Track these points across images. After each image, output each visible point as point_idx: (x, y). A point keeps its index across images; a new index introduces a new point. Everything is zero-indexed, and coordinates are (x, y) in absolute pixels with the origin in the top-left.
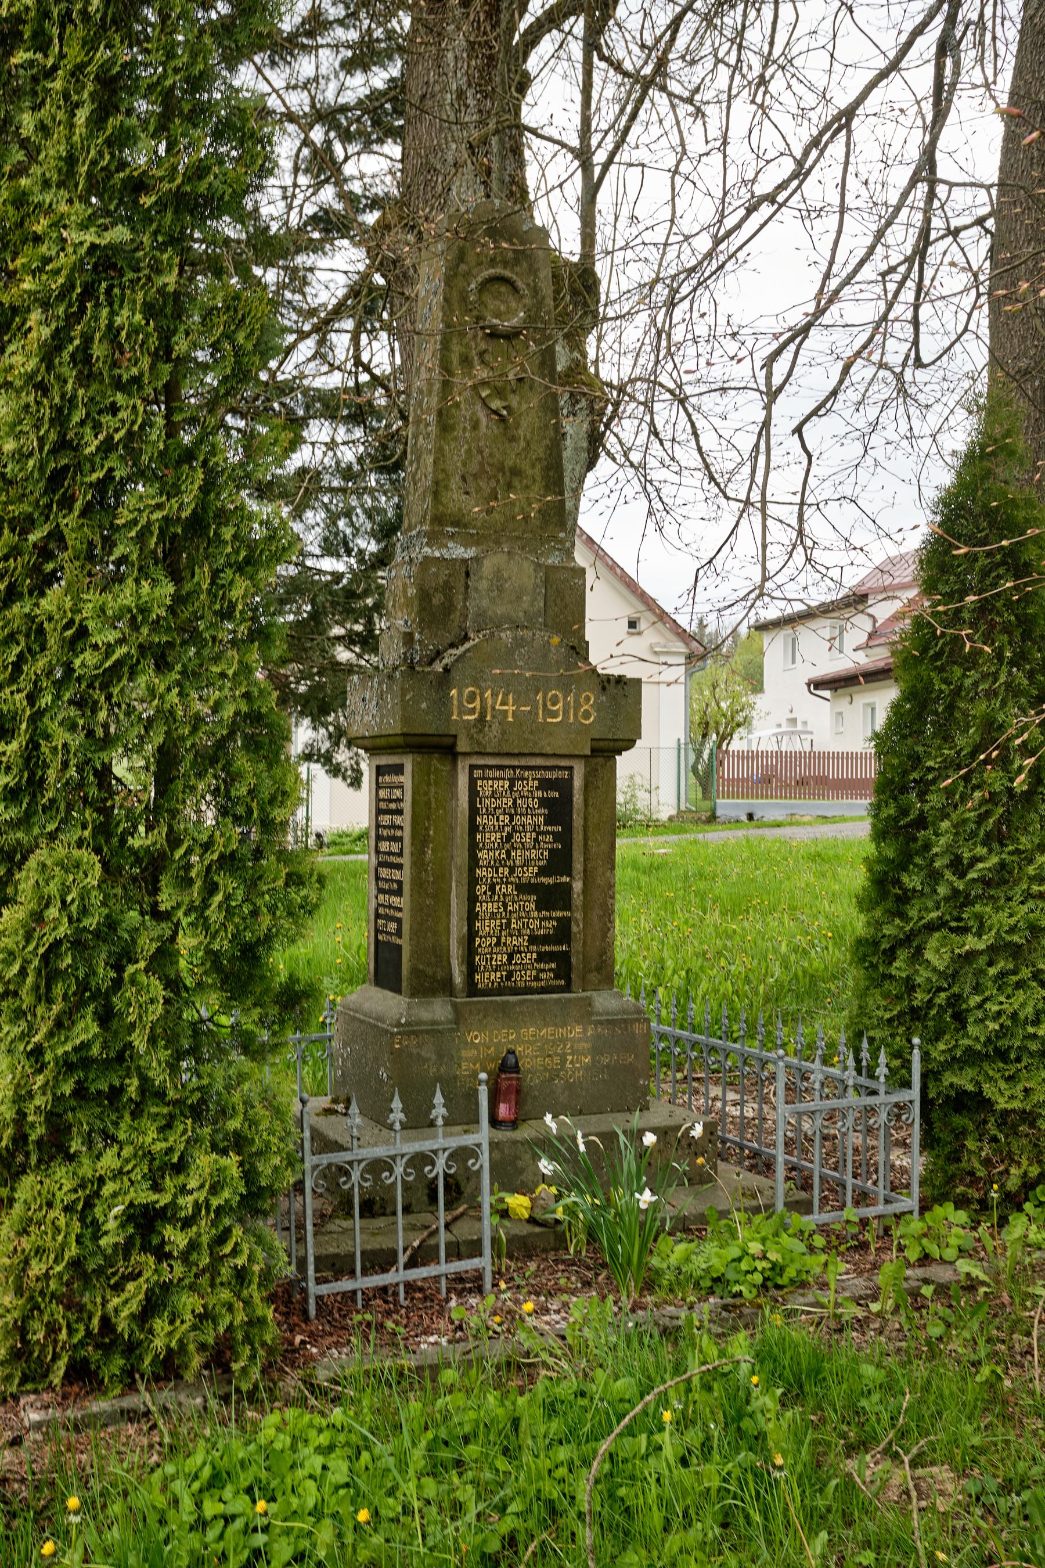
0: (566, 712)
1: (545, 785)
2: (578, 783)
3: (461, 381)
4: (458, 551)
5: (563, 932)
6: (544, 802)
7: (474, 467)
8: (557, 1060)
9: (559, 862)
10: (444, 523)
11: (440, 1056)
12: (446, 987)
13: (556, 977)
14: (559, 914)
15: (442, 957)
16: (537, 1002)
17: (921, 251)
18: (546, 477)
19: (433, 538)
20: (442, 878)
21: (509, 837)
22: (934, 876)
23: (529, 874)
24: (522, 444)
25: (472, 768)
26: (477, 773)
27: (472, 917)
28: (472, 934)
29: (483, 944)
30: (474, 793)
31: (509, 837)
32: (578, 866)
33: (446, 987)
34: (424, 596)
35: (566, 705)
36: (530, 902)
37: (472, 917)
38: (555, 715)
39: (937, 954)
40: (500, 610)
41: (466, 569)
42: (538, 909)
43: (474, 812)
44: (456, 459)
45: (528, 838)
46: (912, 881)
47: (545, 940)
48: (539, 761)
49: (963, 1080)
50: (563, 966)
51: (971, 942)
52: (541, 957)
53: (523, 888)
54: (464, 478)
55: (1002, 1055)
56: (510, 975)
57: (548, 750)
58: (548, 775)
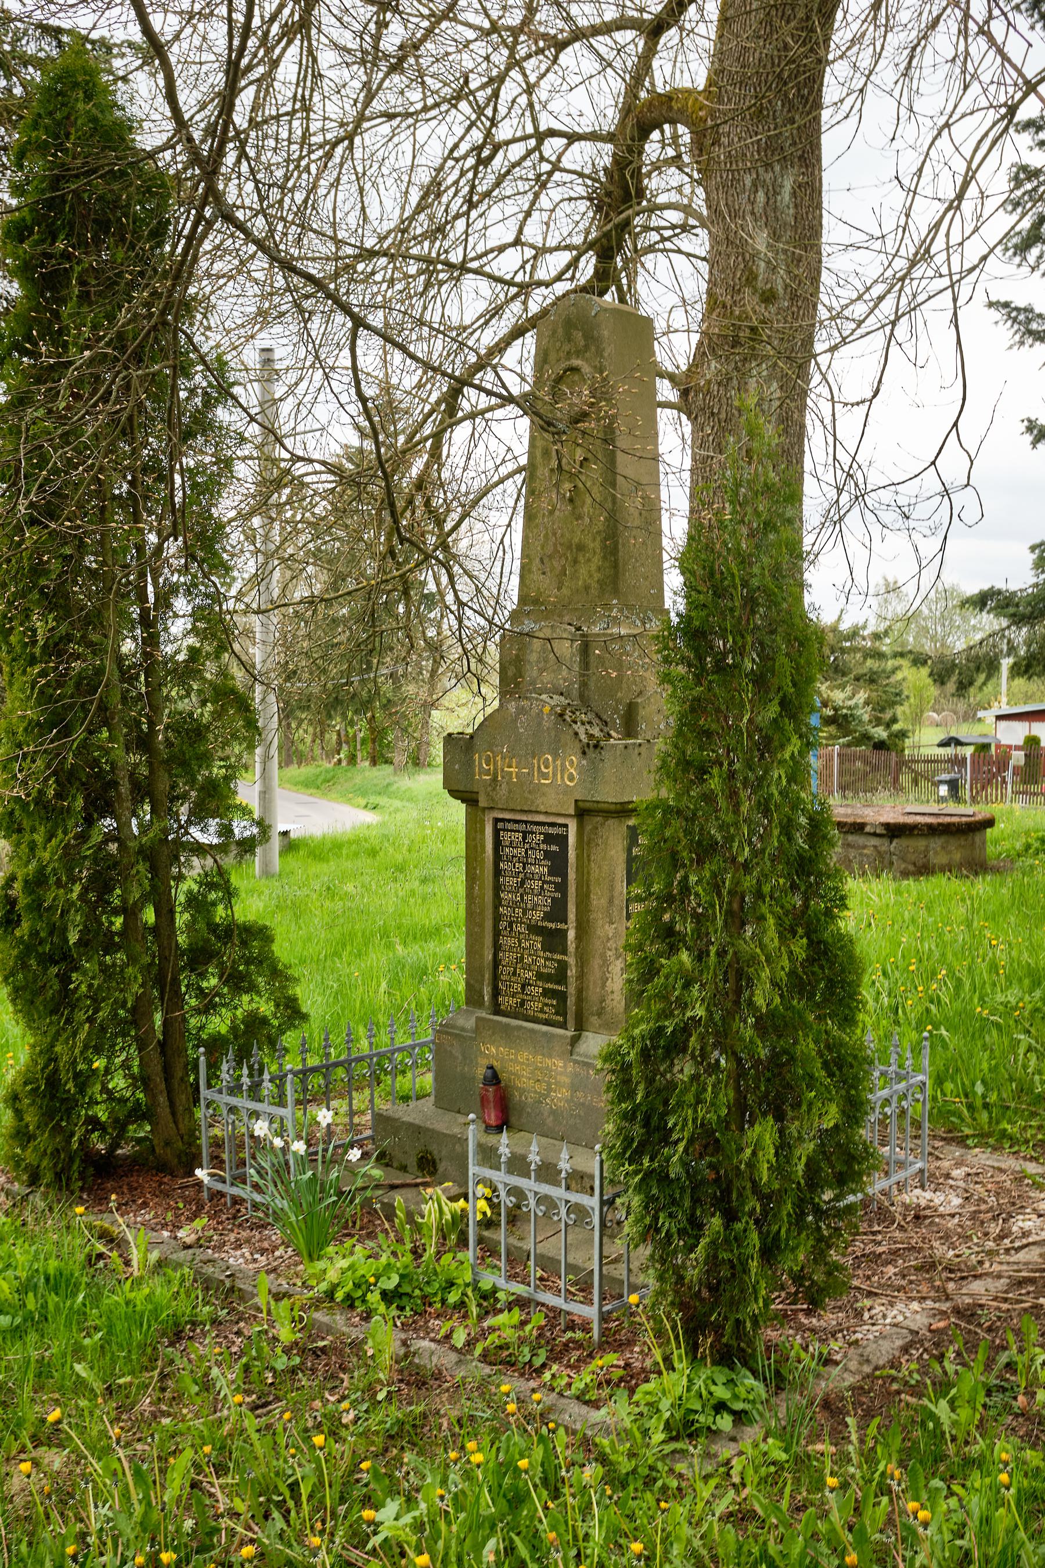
0: (555, 775)
1: (549, 839)
2: (572, 840)
5: (561, 975)
6: (547, 855)
7: (549, 549)
8: (544, 1086)
11: (465, 1058)
13: (557, 1013)
14: (559, 957)
16: (545, 1034)
18: (604, 547)
21: (523, 882)
24: (587, 520)
25: (497, 821)
26: (500, 825)
28: (496, 963)
29: (505, 971)
30: (497, 843)
31: (523, 882)
32: (572, 916)
35: (555, 767)
36: (538, 943)
37: (497, 948)
38: (545, 776)
42: (544, 949)
43: (497, 858)
45: (536, 885)
47: (548, 978)
48: (541, 818)
52: (546, 993)
54: (542, 561)
56: (523, 1003)
57: (542, 808)
58: (551, 830)
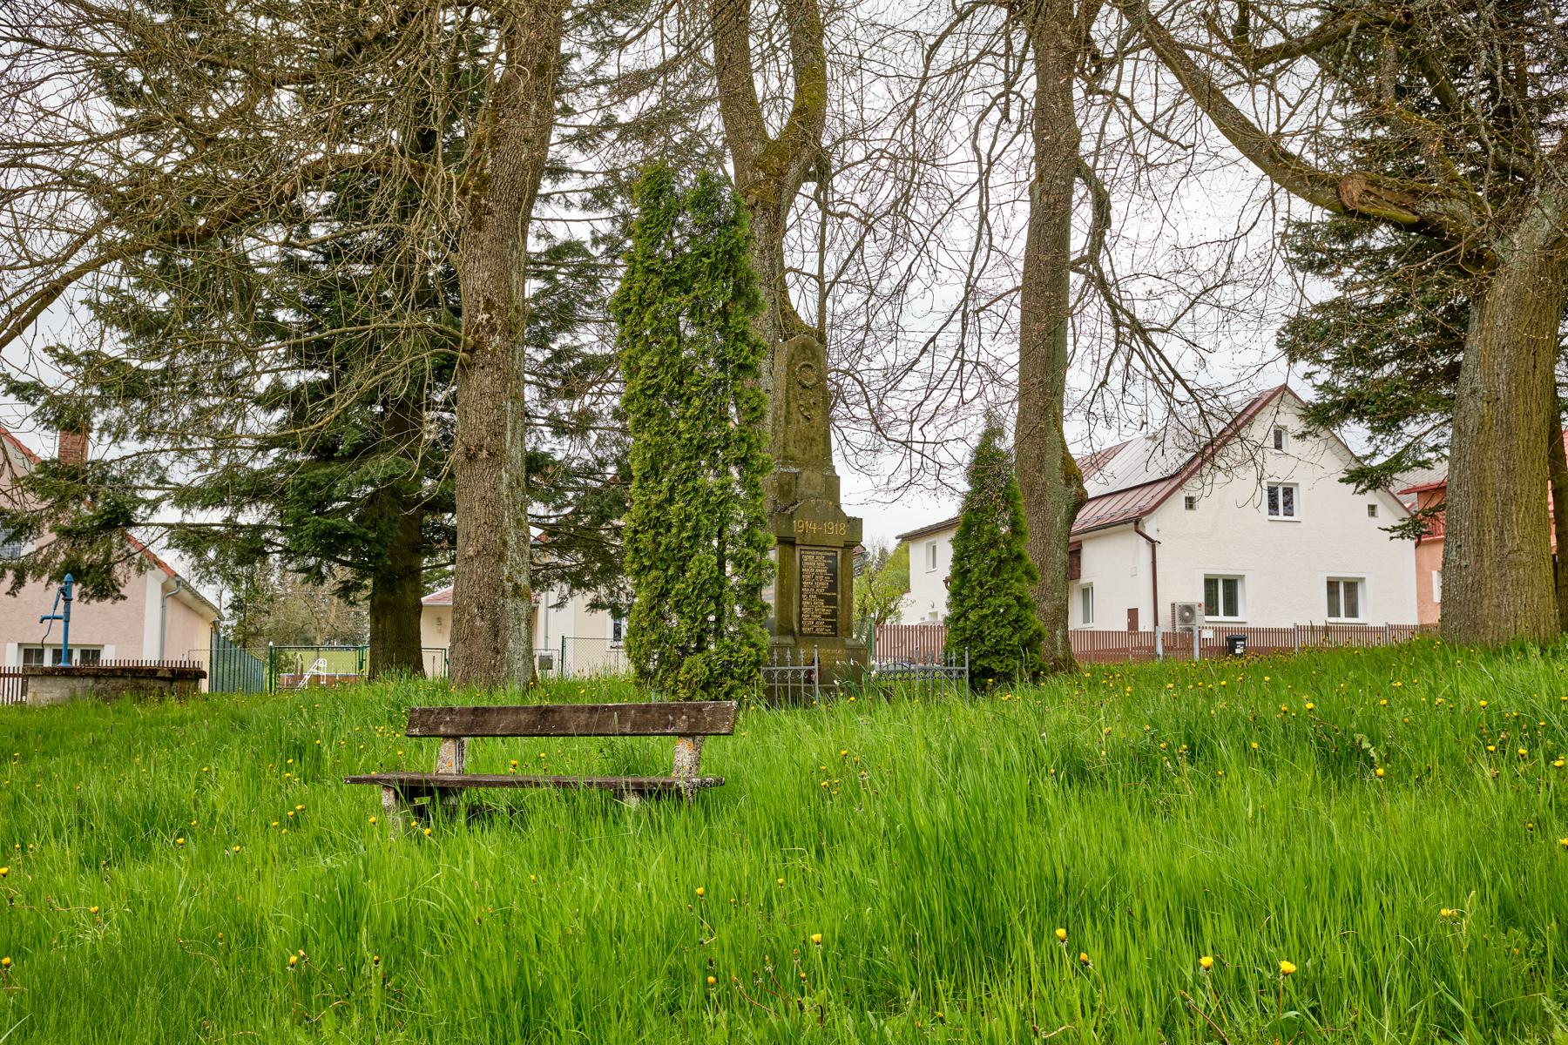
3: (793, 405)
4: (794, 470)
5: (834, 614)
9: (832, 587)
10: (787, 459)
12: (792, 632)
15: (790, 621)
17: (984, 175)
19: (784, 465)
20: (790, 591)
22: (973, 589)
23: (821, 591)
27: (801, 606)
33: (792, 632)
34: (781, 486)
39: (973, 616)
40: (809, 492)
41: (797, 476)
44: (791, 436)
46: (965, 592)
49: (985, 663)
50: (834, 629)
51: (986, 611)
53: (820, 596)
55: (997, 653)
